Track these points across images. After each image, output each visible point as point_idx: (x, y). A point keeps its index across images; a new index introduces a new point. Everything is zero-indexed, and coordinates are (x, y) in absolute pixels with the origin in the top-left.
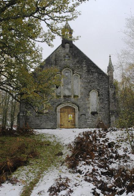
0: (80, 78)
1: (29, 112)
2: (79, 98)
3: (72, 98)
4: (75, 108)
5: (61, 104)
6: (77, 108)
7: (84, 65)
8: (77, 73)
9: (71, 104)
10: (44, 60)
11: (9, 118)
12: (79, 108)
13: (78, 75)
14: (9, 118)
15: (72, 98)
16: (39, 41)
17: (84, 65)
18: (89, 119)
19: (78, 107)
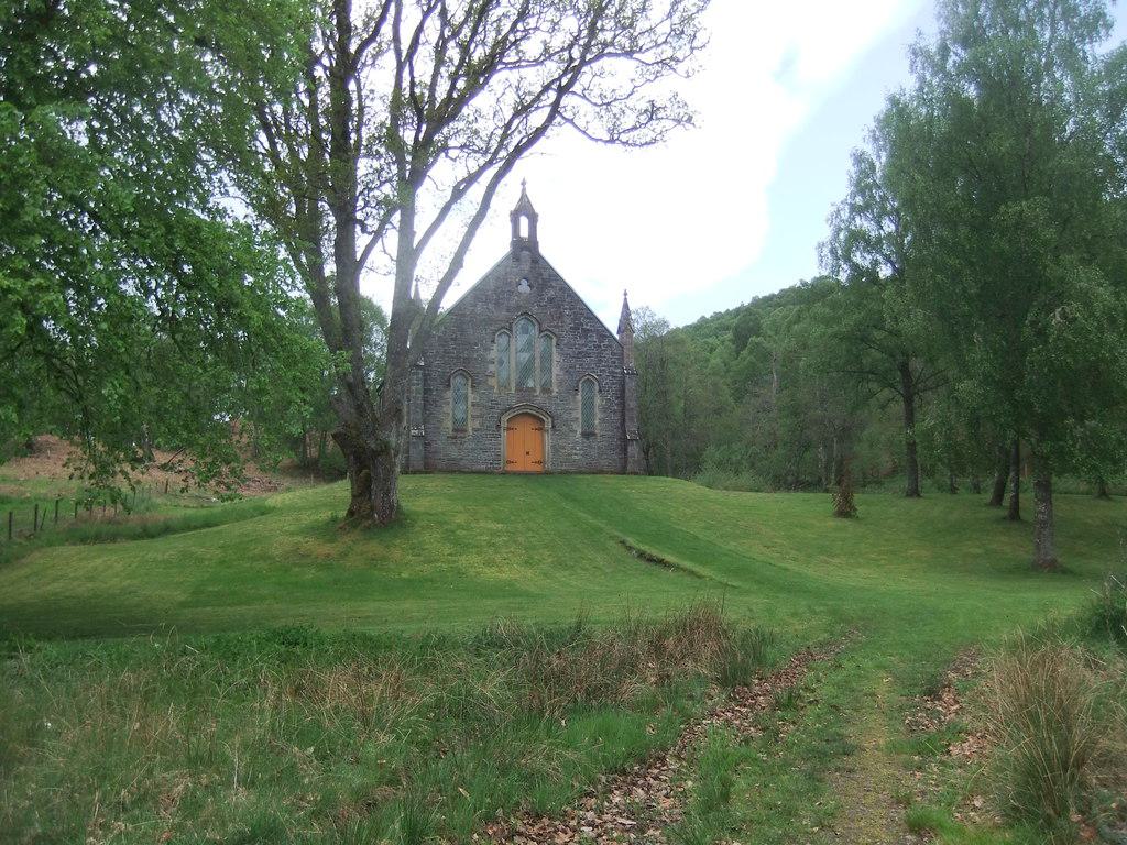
2: (554, 394)
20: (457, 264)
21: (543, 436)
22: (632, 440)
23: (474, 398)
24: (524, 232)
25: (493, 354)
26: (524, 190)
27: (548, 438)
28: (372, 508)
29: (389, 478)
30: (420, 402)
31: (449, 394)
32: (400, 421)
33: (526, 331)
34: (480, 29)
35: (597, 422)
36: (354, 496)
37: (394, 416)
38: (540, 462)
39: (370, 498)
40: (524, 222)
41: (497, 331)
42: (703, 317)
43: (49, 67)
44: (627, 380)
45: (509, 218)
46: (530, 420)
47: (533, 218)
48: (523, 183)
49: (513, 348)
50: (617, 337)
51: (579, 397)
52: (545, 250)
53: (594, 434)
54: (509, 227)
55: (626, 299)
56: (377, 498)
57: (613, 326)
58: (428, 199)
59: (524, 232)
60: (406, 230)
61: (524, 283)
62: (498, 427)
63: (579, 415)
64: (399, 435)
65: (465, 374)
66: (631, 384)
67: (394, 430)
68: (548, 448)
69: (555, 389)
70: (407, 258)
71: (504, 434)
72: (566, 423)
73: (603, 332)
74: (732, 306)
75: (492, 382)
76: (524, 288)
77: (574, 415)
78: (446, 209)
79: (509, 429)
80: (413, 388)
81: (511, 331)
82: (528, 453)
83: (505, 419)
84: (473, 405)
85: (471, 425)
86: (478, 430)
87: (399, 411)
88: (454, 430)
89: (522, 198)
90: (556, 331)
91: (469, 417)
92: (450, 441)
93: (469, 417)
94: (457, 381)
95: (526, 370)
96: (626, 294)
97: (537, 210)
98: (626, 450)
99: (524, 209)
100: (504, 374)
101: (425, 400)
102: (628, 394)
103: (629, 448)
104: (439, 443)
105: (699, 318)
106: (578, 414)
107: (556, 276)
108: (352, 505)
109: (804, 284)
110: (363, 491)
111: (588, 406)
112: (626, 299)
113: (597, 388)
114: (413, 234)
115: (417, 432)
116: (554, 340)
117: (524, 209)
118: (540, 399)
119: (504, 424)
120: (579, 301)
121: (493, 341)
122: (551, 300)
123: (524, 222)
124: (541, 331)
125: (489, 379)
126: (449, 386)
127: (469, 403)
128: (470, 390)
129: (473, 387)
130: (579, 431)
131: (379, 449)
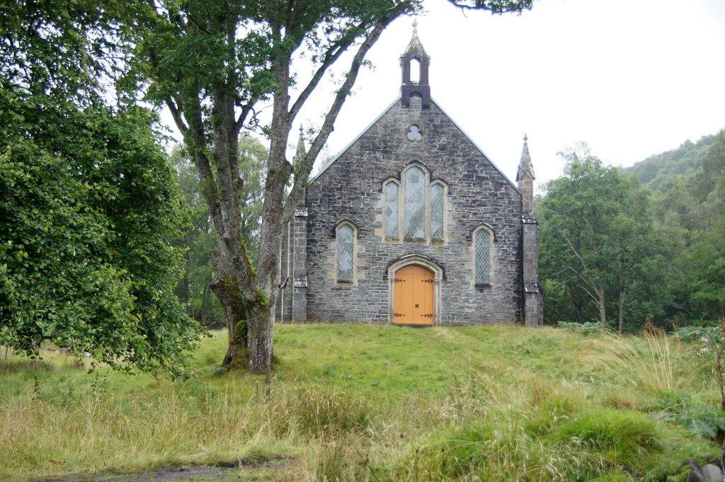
2: (446, 245)
21: (433, 289)
22: (530, 293)
23: (361, 249)
24: (415, 77)
25: (379, 205)
27: (438, 290)
28: (248, 356)
29: (263, 326)
30: (304, 253)
31: (333, 245)
32: (274, 273)
33: (415, 180)
35: (492, 274)
36: (231, 344)
37: (270, 268)
39: (246, 346)
40: (415, 66)
42: (689, 141)
44: (526, 229)
46: (417, 271)
47: (425, 62)
49: (401, 198)
50: (516, 184)
51: (473, 248)
52: (436, 95)
53: (488, 286)
55: (526, 144)
56: (253, 345)
57: (511, 175)
58: (302, 64)
59: (415, 77)
60: (282, 99)
61: (414, 130)
62: (385, 278)
63: (473, 268)
64: (273, 287)
65: (352, 224)
66: (529, 234)
67: (269, 282)
68: (438, 300)
69: (446, 239)
70: (279, 129)
71: (392, 286)
72: (459, 275)
73: (500, 181)
74: (674, 145)
75: (379, 232)
76: (415, 134)
77: (467, 266)
78: (320, 72)
79: (397, 280)
80: (297, 239)
81: (399, 179)
82: (417, 306)
83: (392, 270)
84: (358, 256)
85: (356, 278)
86: (364, 281)
87: (274, 264)
89: (412, 40)
90: (448, 179)
91: (355, 267)
92: (335, 292)
93: (355, 267)
94: (342, 232)
95: (417, 220)
96: (526, 139)
97: (428, 53)
98: (524, 302)
99: (415, 54)
100: (392, 224)
101: (310, 252)
102: (526, 245)
103: (528, 303)
104: (323, 295)
105: (719, 131)
106: (472, 266)
107: (448, 122)
108: (230, 350)
109: (711, 136)
110: (239, 340)
111: (482, 256)
112: (526, 144)
113: (492, 238)
114: (291, 82)
115: (300, 283)
116: (446, 188)
117: (415, 54)
118: (430, 250)
119: (391, 276)
120: (474, 148)
121: (380, 191)
122: (443, 148)
123: (415, 66)
124: (431, 180)
125: (376, 230)
126: (334, 237)
127: (355, 254)
128: (356, 241)
129: (359, 238)
130: (473, 283)
131: (254, 299)
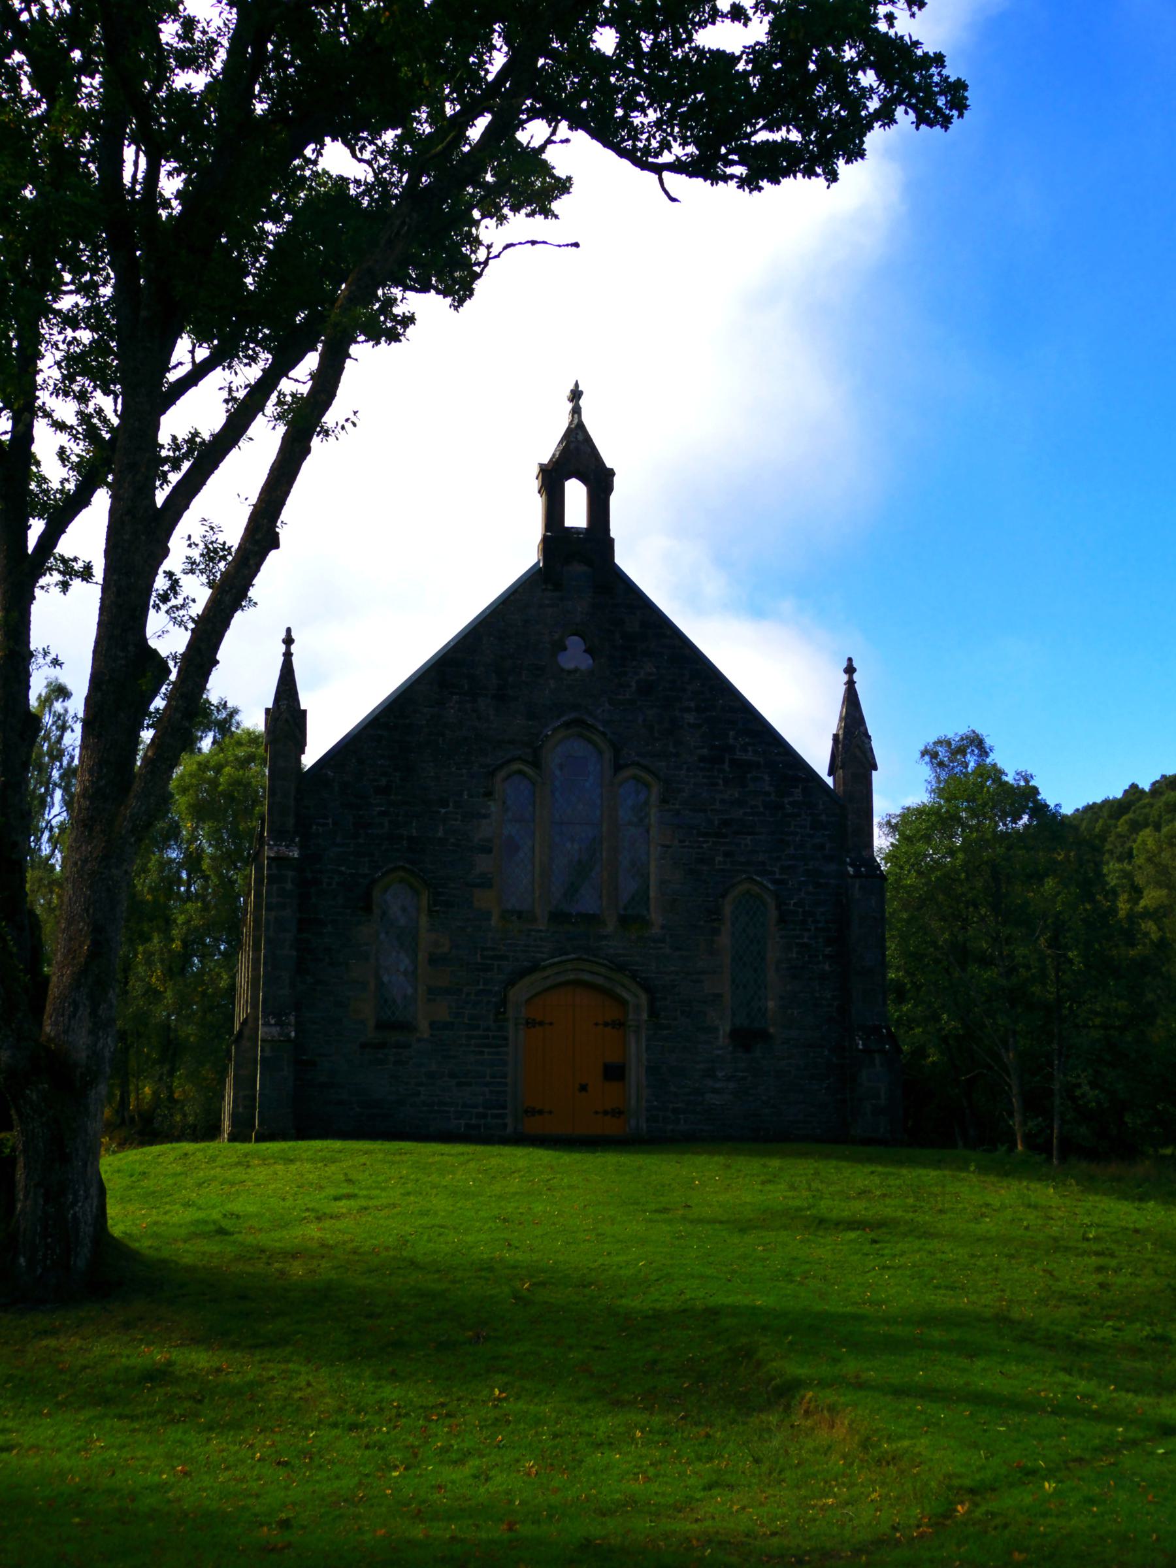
0: (664, 801)
1: (737, 795)
2: (656, 931)
3: (610, 928)
4: (625, 995)
5: (534, 968)
6: (644, 999)
7: (690, 718)
8: (646, 769)
9: (603, 970)
10: (255, 1242)
11: (956, 1335)
12: (652, 1002)
13: (648, 778)
14: (956, 1335)
15: (610, 928)
16: (520, 243)
17: (690, 718)
18: (720, 1074)
19: (648, 988)
20: (789, 1219)
24: (576, 514)
26: (576, 411)
34: (942, 1292)
38: (617, 1113)
40: (576, 494)
41: (501, 767)
43: (172, 861)
45: (535, 484)
48: (576, 395)
51: (724, 940)
54: (536, 506)
59: (576, 514)
61: (575, 644)
69: (656, 917)
82: (583, 1088)
83: (519, 993)
88: (381, 1026)
121: (489, 794)
123: (576, 494)
126: (368, 909)
130: (725, 1028)
